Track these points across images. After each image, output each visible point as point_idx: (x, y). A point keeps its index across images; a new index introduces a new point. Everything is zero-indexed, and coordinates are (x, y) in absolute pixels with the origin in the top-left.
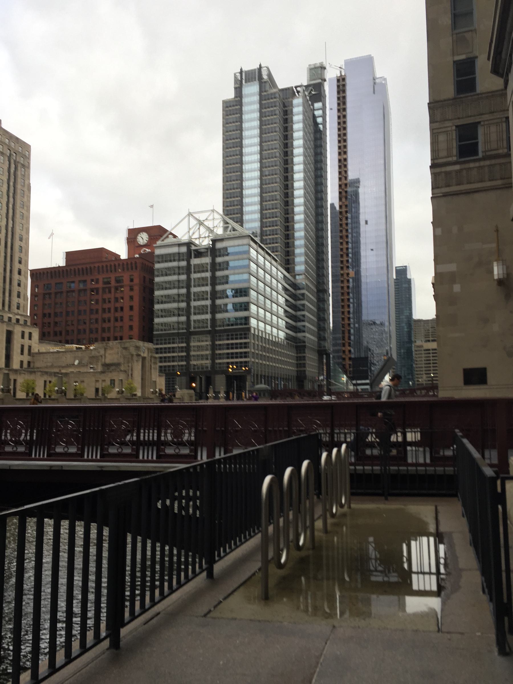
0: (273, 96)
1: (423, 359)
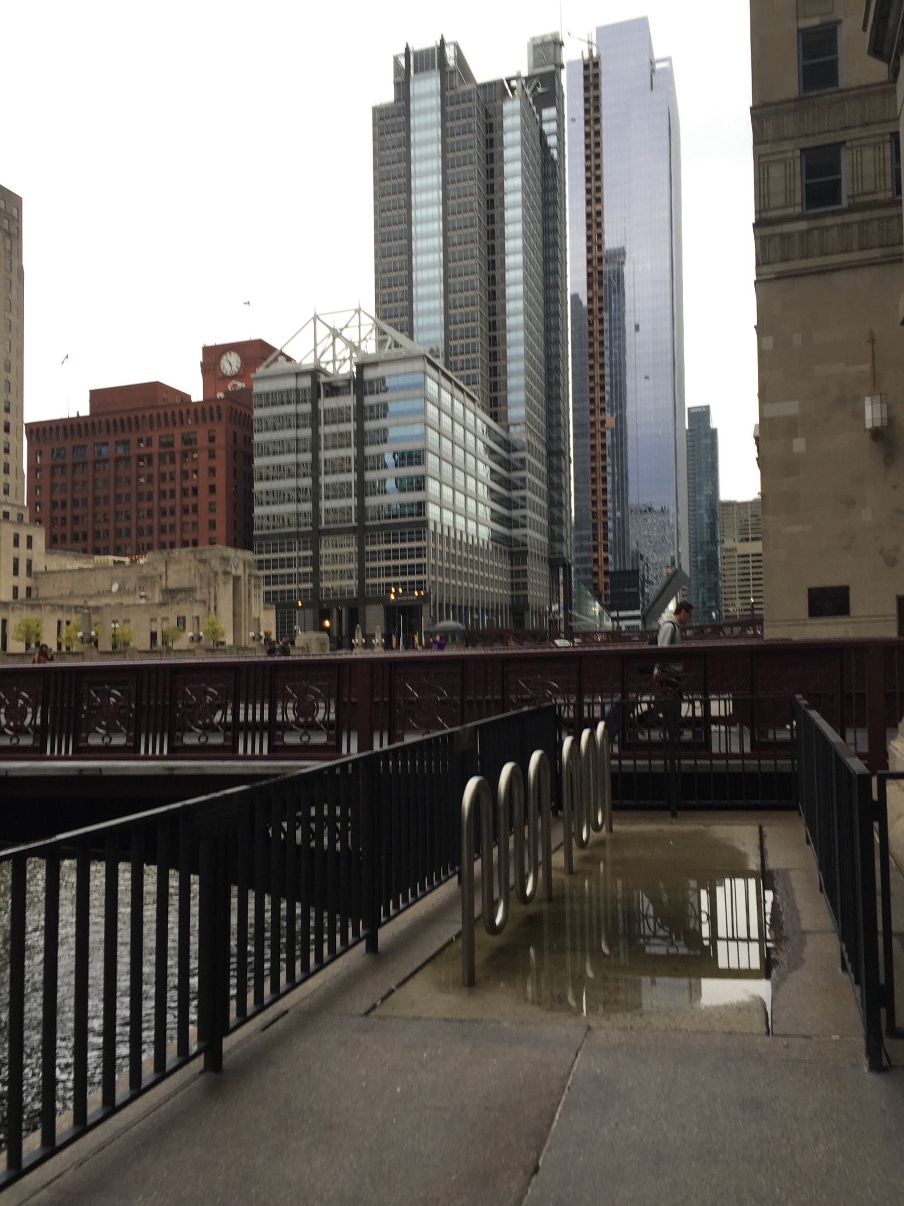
0: (466, 97)
1: (736, 572)
